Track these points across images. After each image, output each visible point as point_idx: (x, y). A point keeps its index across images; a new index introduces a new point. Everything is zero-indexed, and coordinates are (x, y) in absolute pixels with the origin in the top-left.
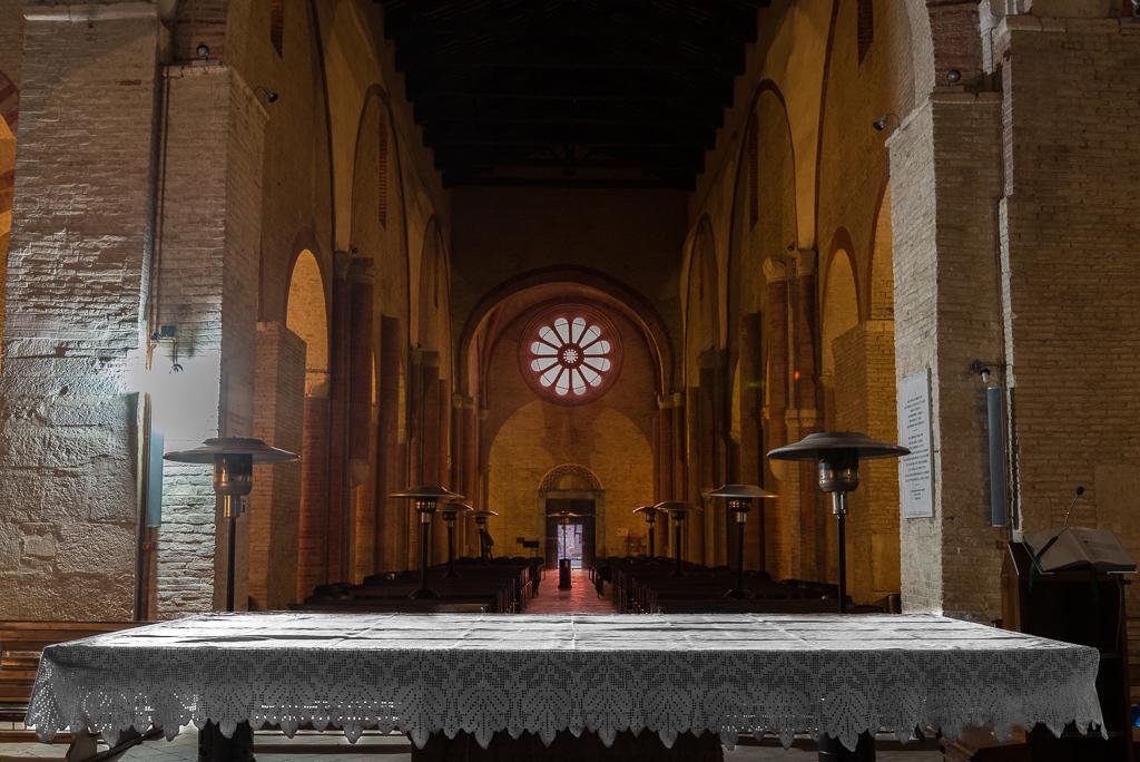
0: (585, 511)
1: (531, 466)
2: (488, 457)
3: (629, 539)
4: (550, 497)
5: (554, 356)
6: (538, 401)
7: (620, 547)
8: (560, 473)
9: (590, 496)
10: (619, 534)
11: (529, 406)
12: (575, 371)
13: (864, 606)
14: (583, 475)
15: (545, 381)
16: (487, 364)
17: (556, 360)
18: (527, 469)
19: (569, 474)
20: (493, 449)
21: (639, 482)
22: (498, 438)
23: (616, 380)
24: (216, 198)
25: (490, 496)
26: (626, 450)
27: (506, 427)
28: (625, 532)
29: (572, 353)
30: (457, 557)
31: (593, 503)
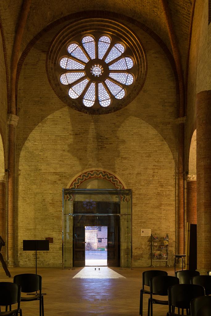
0: (108, 211)
1: (59, 170)
2: (18, 161)
3: (152, 239)
4: (76, 200)
5: (82, 62)
6: (66, 109)
7: (143, 247)
8: (86, 177)
9: (115, 199)
10: (143, 234)
11: (57, 114)
12: (101, 57)
13: (8, 158)
14: (108, 178)
15: (65, 80)
16: (15, 71)
17: (86, 81)
18: (56, 173)
19: (97, 178)
20: (22, 153)
21: (162, 186)
22: (28, 144)
23: (140, 90)
24: (9, 116)
25: (20, 199)
26: (149, 156)
27: (35, 134)
28: (148, 233)
29: (97, 72)
30: (130, 196)
31: (117, 207)
